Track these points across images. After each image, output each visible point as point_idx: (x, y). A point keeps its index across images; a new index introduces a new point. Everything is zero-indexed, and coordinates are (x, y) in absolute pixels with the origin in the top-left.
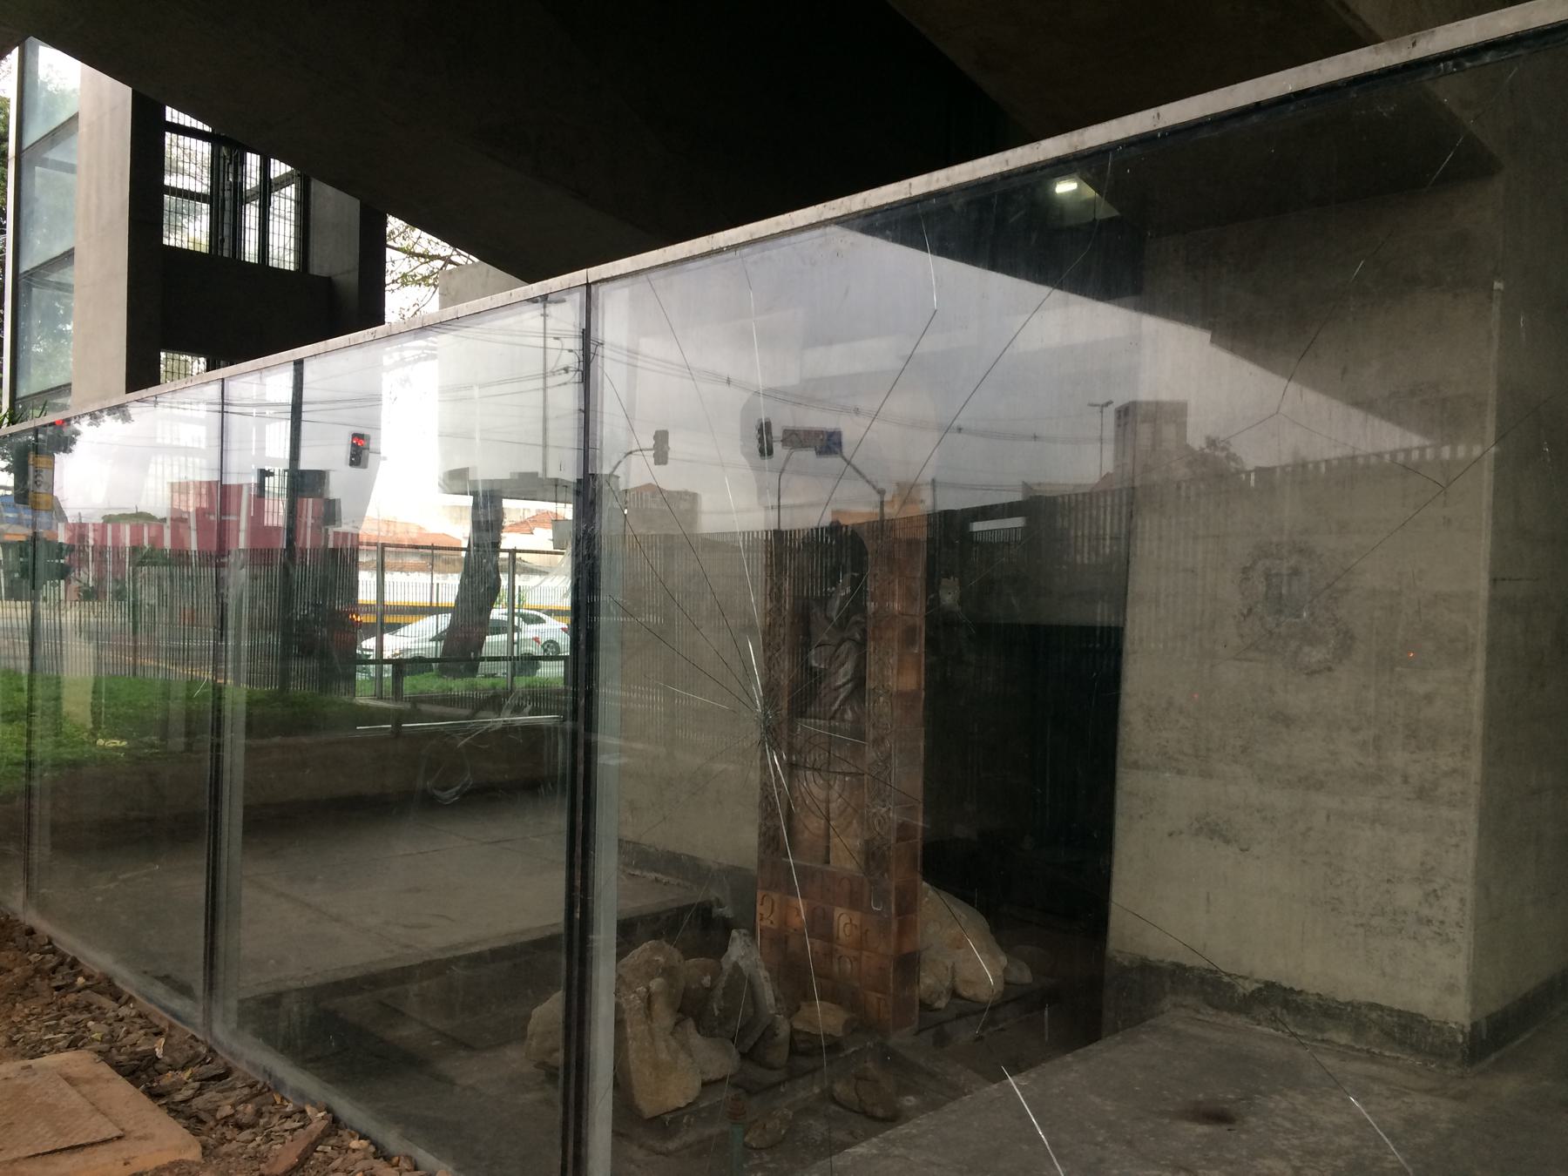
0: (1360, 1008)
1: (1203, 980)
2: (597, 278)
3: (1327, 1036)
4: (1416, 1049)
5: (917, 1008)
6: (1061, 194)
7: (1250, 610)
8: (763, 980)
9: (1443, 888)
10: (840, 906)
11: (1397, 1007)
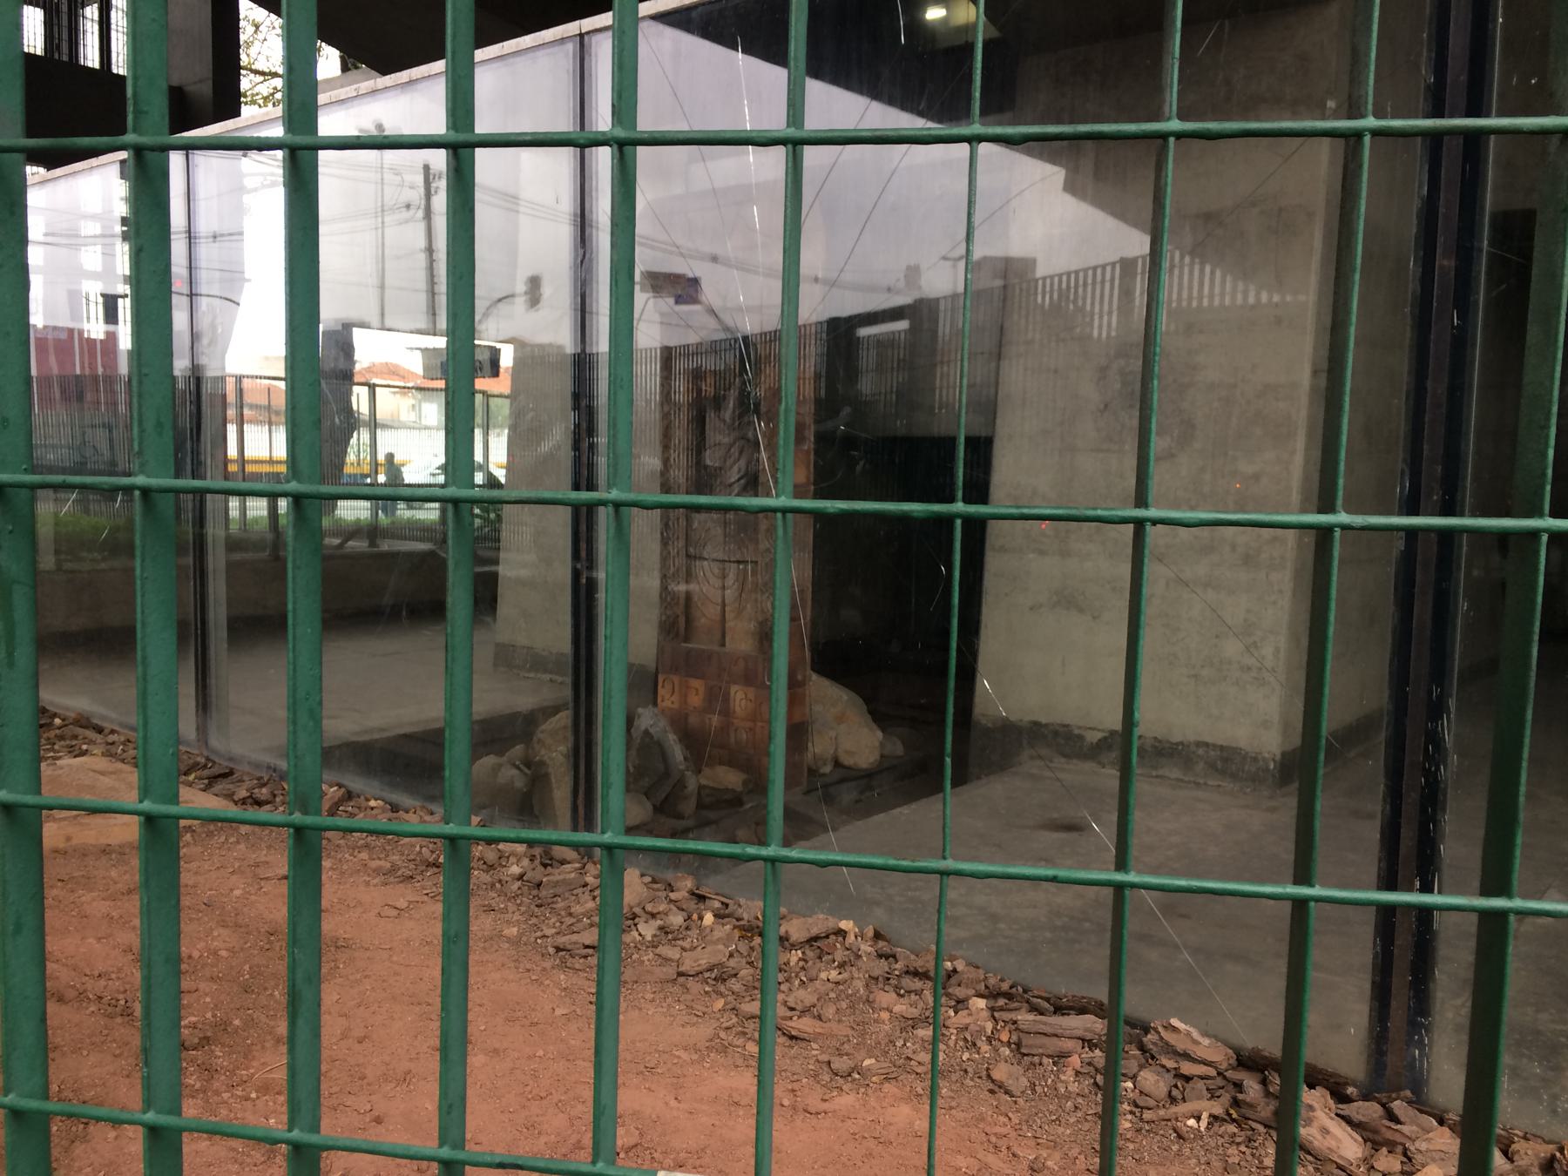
0: (1188, 746)
1: (1056, 733)
2: (591, 28)
3: (1160, 772)
4: (1234, 777)
5: (806, 775)
6: (934, 21)
7: (1106, 406)
8: (672, 742)
10: (735, 683)
11: (1220, 743)
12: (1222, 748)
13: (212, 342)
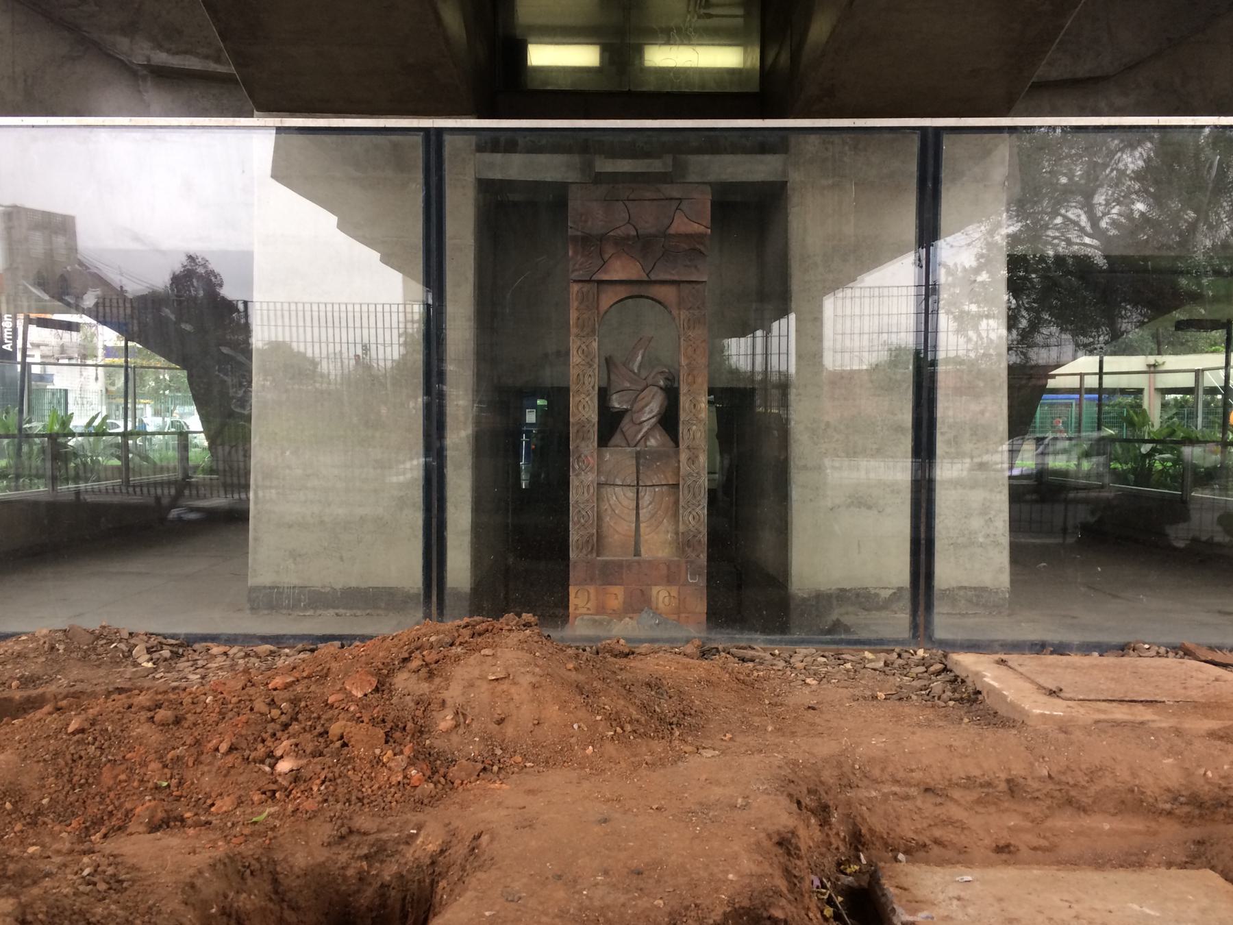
1: (858, 595)
9: (995, 516)
11: (973, 585)
12: (975, 589)
13: (136, 238)
